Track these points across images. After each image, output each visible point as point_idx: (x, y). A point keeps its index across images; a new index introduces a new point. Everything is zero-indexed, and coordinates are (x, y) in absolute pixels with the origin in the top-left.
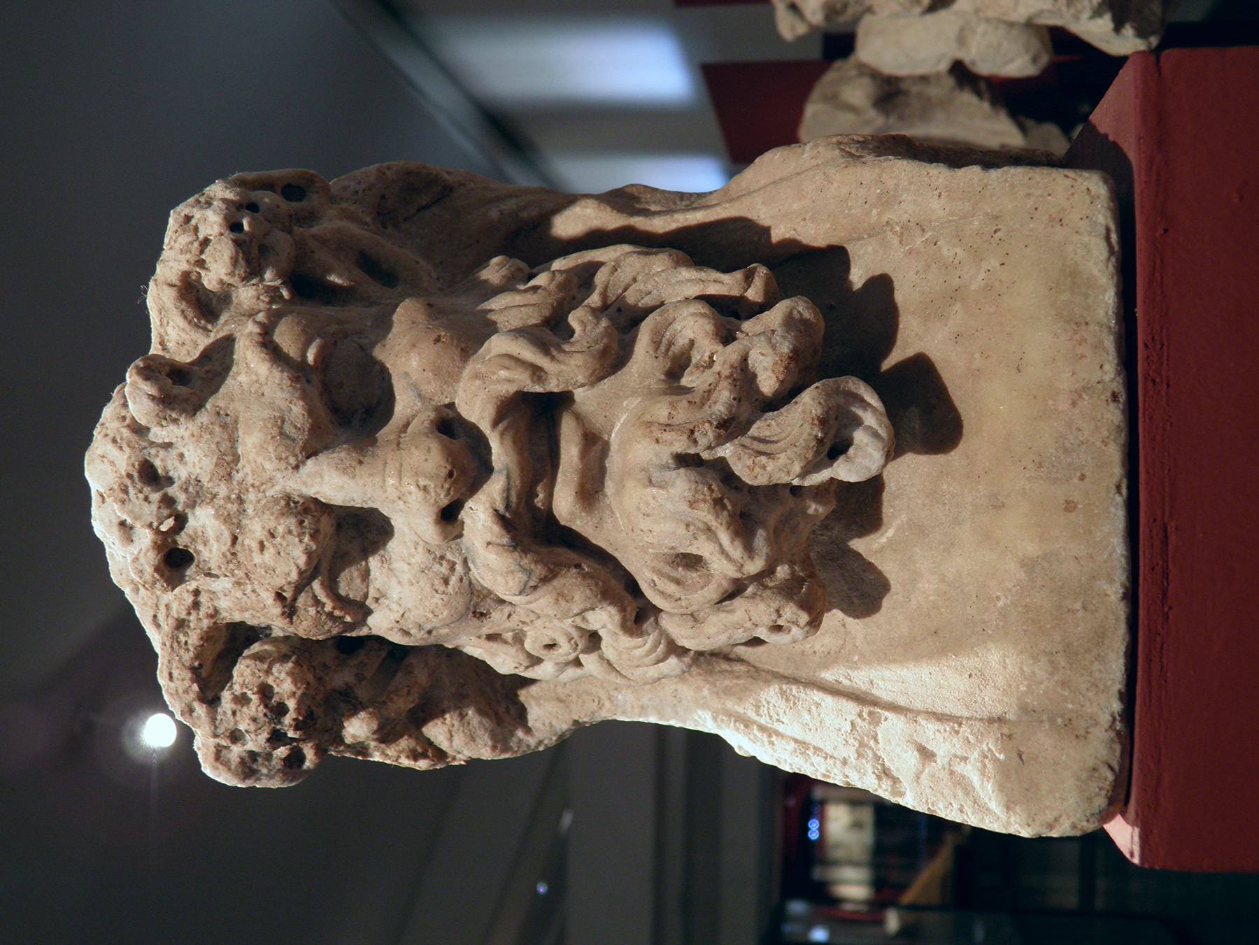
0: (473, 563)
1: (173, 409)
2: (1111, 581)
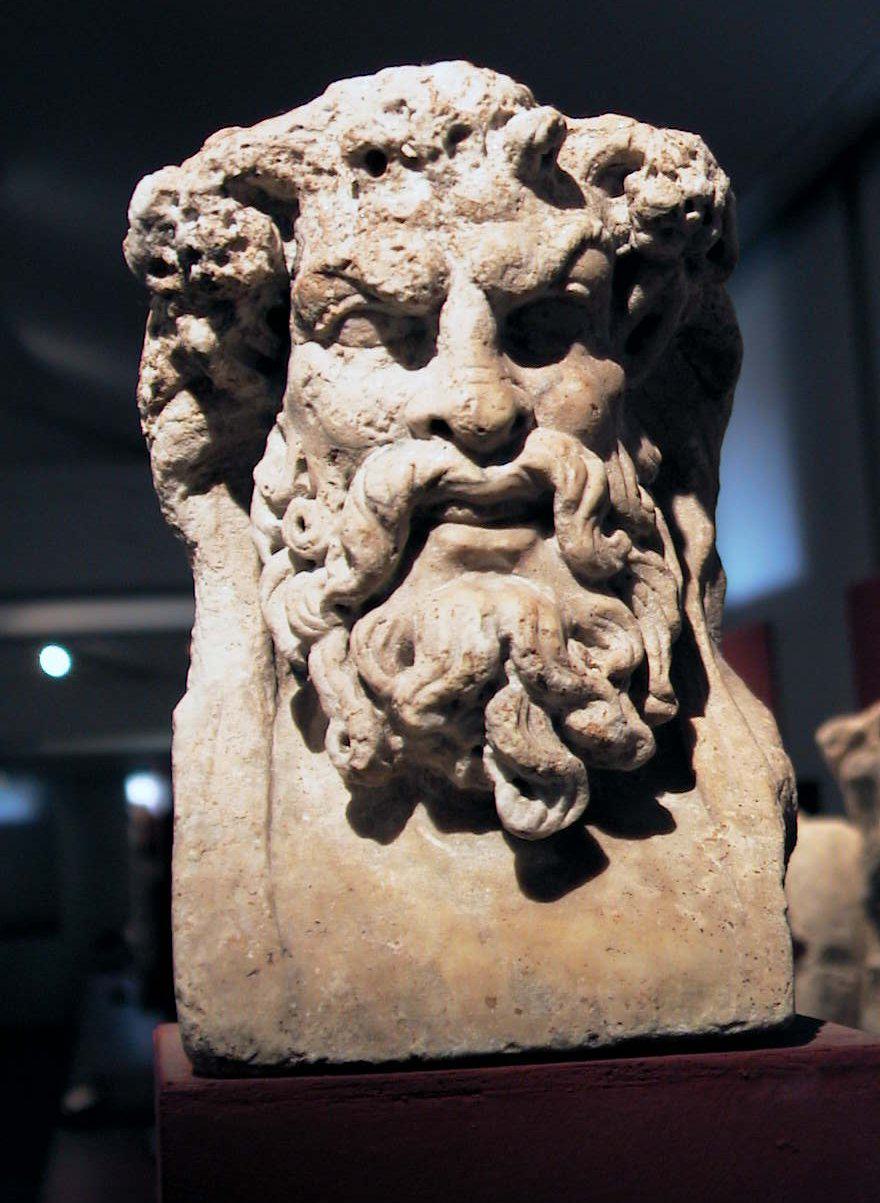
0: (390, 449)
1: (521, 157)
2: (428, 1044)
